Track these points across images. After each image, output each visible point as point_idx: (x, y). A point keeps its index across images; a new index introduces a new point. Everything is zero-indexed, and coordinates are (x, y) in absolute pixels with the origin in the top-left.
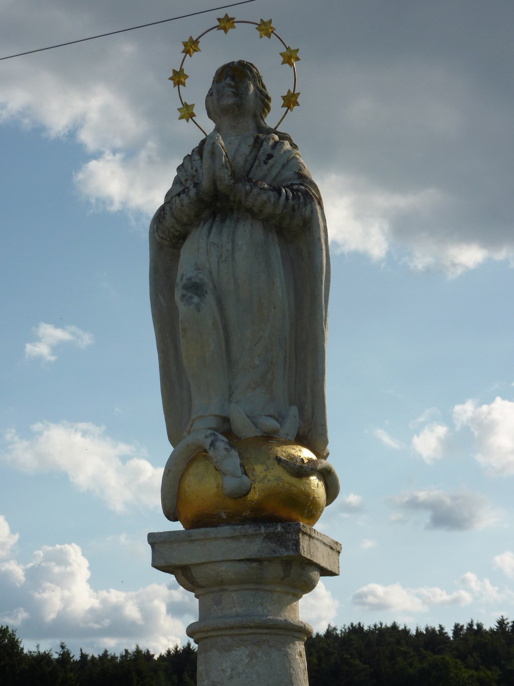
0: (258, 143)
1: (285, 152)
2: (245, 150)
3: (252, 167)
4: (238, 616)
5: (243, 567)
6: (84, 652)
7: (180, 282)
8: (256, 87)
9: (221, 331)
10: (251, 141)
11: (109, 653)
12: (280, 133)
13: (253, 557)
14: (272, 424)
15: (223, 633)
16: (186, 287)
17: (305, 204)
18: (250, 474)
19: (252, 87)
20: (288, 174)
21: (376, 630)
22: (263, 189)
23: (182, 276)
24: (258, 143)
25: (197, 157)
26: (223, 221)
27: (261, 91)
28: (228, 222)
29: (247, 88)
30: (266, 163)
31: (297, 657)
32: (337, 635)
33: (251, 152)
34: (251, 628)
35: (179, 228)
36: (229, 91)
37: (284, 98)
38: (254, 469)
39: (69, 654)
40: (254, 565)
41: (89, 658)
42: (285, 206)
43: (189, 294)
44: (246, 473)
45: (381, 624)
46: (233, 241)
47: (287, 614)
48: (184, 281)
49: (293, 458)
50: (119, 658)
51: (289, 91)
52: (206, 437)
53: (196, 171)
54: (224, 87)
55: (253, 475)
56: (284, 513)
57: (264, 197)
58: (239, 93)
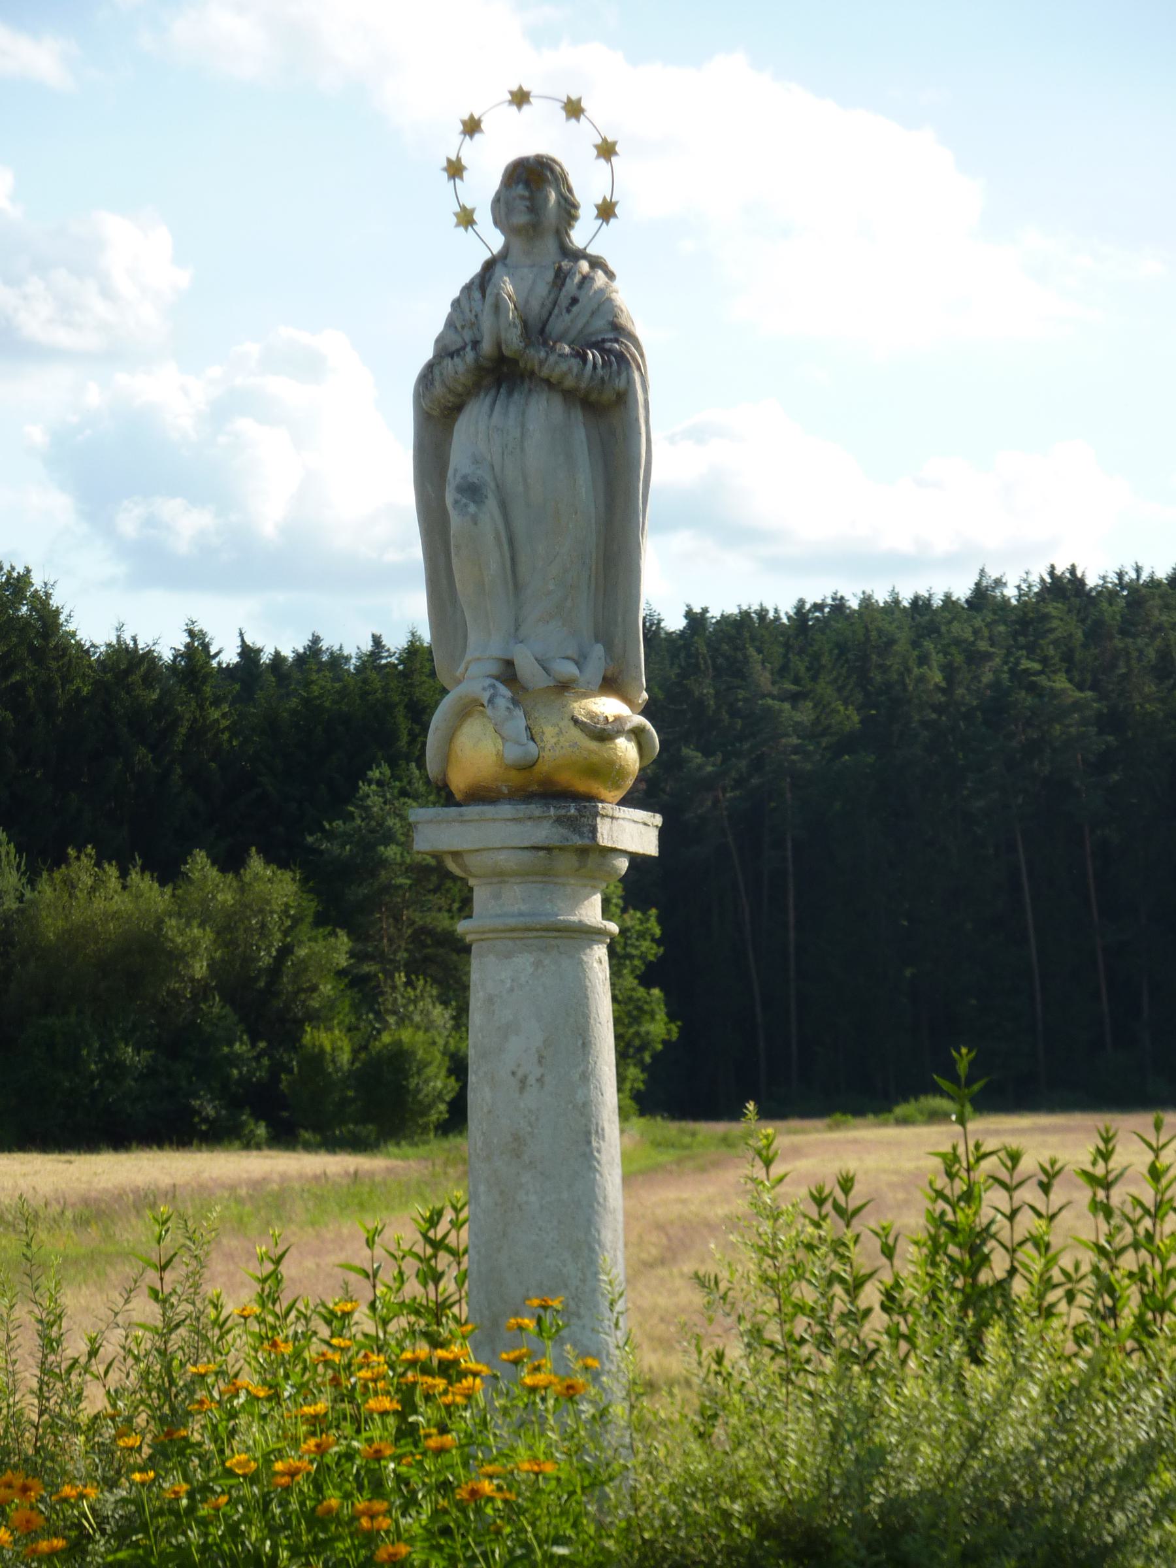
0: (561, 277)
1: (595, 292)
2: (542, 289)
3: (550, 314)
4: (521, 914)
5: (527, 856)
6: (249, 642)
7: (452, 480)
8: (560, 194)
9: (506, 547)
10: (550, 275)
11: (324, 645)
12: (591, 256)
13: (540, 845)
14: (568, 669)
15: (503, 935)
16: (461, 489)
17: (619, 373)
18: (537, 739)
19: (553, 196)
20: (600, 323)
21: (1123, 589)
22: (561, 356)
23: (456, 470)
24: (561, 277)
25: (477, 295)
26: (510, 393)
27: (566, 199)
28: (516, 396)
29: (546, 199)
30: (568, 311)
31: (595, 965)
32: (1006, 601)
33: (550, 292)
34: (537, 930)
35: (452, 399)
36: (521, 205)
37: (598, 207)
38: (543, 733)
39: (206, 647)
40: (541, 853)
41: (265, 658)
42: (592, 378)
43: (464, 501)
44: (533, 739)
45: (1138, 570)
46: (523, 425)
47: (583, 912)
48: (458, 479)
49: (592, 716)
50: (353, 661)
51: (605, 198)
52: (484, 689)
53: (476, 316)
54: (514, 199)
55: (542, 741)
56: (582, 786)
57: (564, 367)
58: (535, 207)
